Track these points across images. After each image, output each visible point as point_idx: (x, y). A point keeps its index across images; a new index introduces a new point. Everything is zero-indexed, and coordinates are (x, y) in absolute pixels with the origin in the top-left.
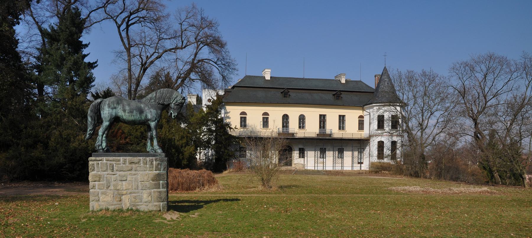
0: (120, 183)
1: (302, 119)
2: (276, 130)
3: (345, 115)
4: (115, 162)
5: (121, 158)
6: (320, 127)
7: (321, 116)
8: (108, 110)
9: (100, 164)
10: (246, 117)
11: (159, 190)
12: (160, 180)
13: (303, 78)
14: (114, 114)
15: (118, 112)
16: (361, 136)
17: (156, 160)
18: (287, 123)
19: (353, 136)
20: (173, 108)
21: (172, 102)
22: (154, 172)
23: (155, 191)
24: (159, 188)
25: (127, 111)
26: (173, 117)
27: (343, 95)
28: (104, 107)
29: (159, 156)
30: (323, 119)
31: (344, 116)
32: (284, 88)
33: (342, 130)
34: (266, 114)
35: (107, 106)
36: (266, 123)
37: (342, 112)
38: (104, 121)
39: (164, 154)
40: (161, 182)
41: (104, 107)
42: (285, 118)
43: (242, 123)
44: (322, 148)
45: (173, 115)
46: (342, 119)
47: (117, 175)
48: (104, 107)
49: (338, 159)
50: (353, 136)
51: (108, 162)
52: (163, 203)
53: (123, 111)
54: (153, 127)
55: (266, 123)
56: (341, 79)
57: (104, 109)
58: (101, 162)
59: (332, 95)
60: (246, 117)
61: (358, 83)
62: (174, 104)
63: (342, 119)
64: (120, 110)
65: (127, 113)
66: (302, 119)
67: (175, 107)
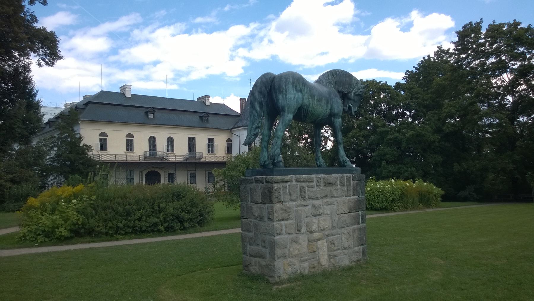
0: (315, 220)
1: (170, 142)
2: (142, 153)
3: (214, 138)
4: (308, 184)
5: (314, 176)
6: (190, 150)
7: (189, 138)
8: (292, 92)
9: (288, 187)
10: (107, 138)
11: (358, 226)
12: (359, 210)
13: (166, 98)
14: (300, 101)
15: (304, 97)
16: (206, 159)
17: (354, 179)
18: (155, 146)
19: (224, 159)
20: (353, 100)
21: (352, 91)
22: (352, 197)
23: (354, 227)
24: (359, 223)
25: (315, 97)
26: (353, 113)
27: (211, 118)
28: (286, 86)
29: (354, 172)
30: (192, 142)
31: (213, 139)
32: (148, 108)
33: (211, 153)
34: (130, 135)
35: (291, 86)
36: (130, 146)
37: (211, 135)
38: (287, 111)
39: (359, 169)
40: (360, 213)
41: (286, 86)
42: (152, 141)
43: (128, 142)
44: (194, 172)
45: (353, 110)
46: (211, 141)
47: (310, 207)
48: (287, 87)
49: (209, 184)
50: (224, 159)
51: (299, 184)
52: (363, 246)
53: (311, 97)
54: (339, 127)
55: (130, 146)
56: (206, 101)
57: (286, 91)
58: (289, 183)
59: (199, 117)
60: (107, 138)
61: (223, 106)
62: (354, 93)
63: (211, 141)
64: (307, 95)
65: (316, 100)
66: (170, 142)
67: (356, 99)
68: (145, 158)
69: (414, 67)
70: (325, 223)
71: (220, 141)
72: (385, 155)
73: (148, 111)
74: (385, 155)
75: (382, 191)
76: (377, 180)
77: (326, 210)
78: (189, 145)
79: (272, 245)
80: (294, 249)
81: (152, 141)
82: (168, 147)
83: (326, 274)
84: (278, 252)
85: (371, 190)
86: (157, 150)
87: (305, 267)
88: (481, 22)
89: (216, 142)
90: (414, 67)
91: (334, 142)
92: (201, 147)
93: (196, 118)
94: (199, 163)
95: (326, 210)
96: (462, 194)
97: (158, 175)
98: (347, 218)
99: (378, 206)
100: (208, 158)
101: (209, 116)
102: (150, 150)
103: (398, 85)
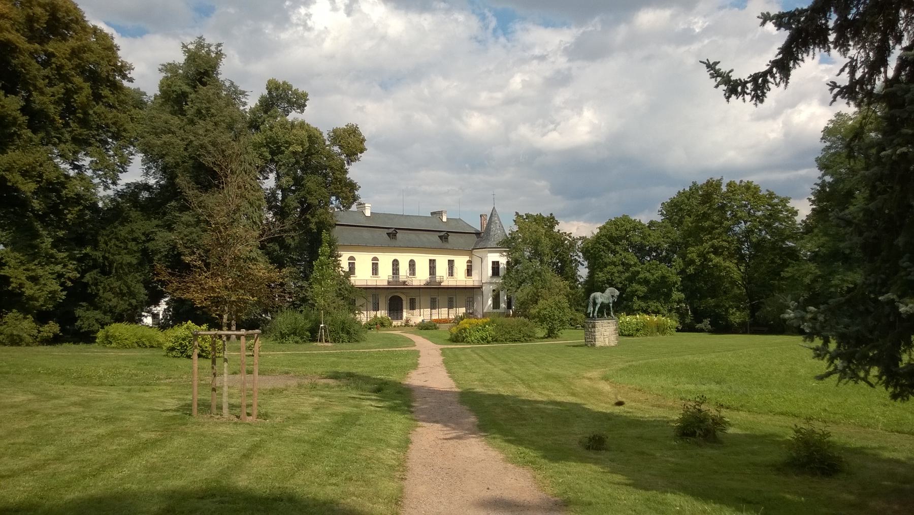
18: (398, 269)
42: (395, 263)
68: (389, 282)
69: (717, 86)
70: (608, 333)
71: (461, 262)
72: (636, 291)
73: (393, 234)
74: (636, 291)
75: (629, 323)
76: (627, 315)
77: (608, 330)
78: (430, 267)
79: (595, 339)
80: (600, 340)
81: (395, 263)
82: (410, 270)
83: (607, 347)
84: (597, 340)
85: (623, 322)
86: (400, 274)
87: (602, 345)
88: (722, 179)
89: (456, 264)
90: (717, 86)
91: (588, 267)
92: (442, 269)
93: (435, 238)
94: (440, 288)
95: (608, 330)
96: (698, 326)
97: (400, 300)
98: (613, 332)
99: (627, 333)
100: (448, 282)
101: (448, 235)
102: (393, 274)
103: (652, 224)
